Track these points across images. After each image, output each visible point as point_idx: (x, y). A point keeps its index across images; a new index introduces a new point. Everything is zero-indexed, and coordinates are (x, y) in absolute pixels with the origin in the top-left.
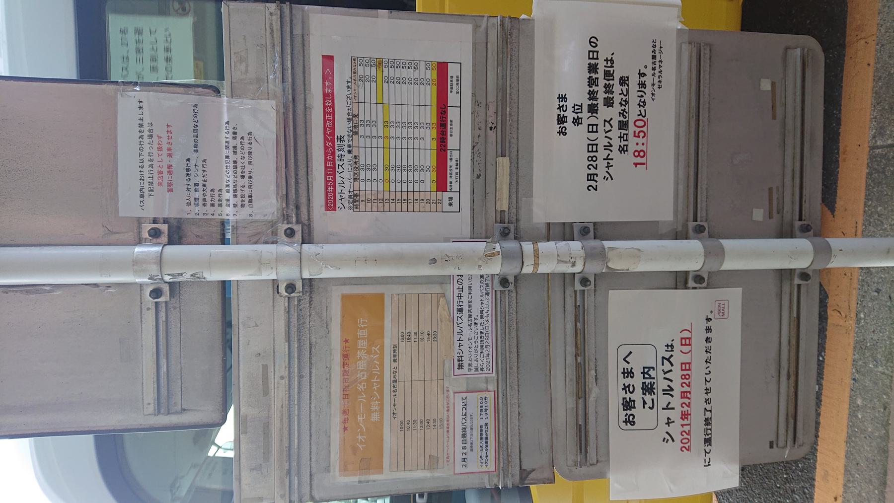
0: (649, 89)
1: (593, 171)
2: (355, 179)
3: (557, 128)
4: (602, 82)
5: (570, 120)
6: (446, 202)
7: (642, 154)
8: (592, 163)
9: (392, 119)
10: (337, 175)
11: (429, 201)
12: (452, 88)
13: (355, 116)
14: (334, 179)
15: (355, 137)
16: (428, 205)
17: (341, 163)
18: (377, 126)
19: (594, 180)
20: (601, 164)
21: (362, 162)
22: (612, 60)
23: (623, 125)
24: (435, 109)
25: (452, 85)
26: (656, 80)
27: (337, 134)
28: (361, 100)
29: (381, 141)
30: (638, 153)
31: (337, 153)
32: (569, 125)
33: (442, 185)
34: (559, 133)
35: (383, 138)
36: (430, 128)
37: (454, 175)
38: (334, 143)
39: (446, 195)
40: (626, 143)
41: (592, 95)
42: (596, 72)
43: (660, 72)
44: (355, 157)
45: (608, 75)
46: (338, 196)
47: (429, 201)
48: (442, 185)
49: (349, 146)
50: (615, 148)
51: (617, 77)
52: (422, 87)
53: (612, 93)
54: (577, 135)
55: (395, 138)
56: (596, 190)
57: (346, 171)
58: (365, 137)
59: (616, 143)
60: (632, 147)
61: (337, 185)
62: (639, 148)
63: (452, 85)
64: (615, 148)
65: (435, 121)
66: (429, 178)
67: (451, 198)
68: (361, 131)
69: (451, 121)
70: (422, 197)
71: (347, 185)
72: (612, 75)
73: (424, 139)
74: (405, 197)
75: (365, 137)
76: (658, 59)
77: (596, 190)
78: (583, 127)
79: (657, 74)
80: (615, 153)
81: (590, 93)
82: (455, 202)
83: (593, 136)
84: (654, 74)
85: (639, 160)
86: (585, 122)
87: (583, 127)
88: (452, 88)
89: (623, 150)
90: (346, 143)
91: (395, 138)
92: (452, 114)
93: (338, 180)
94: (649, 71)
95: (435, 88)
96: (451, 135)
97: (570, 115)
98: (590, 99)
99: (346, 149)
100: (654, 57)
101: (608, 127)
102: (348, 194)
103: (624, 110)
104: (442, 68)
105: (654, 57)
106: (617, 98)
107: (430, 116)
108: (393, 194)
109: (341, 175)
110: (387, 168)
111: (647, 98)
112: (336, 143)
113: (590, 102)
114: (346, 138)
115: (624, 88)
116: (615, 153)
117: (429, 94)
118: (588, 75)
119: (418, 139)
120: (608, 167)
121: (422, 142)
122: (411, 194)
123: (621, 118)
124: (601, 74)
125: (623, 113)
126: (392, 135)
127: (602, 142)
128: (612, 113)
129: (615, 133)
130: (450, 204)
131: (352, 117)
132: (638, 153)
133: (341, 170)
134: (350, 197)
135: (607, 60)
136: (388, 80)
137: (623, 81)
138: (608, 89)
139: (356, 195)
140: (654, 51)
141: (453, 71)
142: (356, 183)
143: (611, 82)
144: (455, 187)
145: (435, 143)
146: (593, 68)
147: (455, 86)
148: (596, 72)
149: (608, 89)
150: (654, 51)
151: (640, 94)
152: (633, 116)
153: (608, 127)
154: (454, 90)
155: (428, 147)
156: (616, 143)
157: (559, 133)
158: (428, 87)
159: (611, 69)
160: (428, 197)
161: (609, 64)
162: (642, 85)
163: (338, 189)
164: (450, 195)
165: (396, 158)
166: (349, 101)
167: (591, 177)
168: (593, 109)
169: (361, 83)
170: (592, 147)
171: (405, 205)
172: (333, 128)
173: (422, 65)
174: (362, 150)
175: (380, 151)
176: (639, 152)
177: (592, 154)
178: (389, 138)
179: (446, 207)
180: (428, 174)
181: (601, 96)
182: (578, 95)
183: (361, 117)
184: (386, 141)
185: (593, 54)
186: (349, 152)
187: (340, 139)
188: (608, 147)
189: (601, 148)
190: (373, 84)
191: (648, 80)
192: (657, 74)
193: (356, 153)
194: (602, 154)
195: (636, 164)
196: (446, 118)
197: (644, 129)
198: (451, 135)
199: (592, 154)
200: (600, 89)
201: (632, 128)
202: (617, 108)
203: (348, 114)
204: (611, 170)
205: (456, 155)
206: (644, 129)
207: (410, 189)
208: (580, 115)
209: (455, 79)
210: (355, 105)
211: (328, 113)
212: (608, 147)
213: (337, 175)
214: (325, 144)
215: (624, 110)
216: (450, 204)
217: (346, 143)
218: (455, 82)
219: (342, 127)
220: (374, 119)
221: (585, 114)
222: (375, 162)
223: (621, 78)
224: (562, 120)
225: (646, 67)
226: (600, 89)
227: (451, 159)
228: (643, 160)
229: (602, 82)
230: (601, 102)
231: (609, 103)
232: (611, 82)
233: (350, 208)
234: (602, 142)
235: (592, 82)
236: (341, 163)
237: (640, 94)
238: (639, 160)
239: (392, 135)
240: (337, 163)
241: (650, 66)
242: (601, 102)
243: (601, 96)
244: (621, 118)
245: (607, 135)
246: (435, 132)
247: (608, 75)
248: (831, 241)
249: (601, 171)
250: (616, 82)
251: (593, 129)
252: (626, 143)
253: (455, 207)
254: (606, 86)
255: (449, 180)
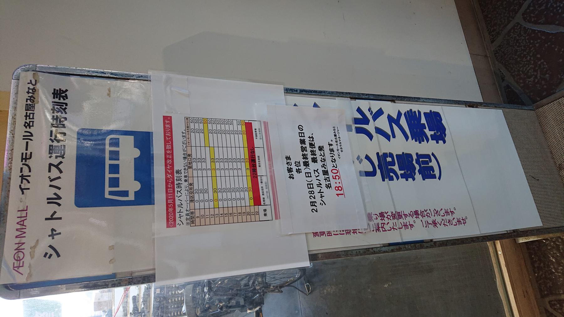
0: (336, 152)
1: (313, 200)
2: (191, 201)
3: (288, 175)
4: (309, 149)
5: (294, 170)
6: (262, 213)
7: (340, 188)
8: (311, 195)
9: (217, 157)
10: (177, 198)
11: (249, 214)
12: (256, 136)
13: (189, 155)
14: (174, 201)
15: (190, 170)
16: (249, 217)
17: (179, 190)
18: (206, 162)
19: (314, 205)
20: (318, 196)
21: (196, 187)
22: (312, 137)
23: (325, 173)
24: (246, 150)
25: (256, 134)
26: (339, 147)
27: (176, 168)
28: (193, 144)
29: (209, 172)
30: (338, 188)
31: (176, 182)
32: (294, 172)
33: (257, 201)
34: (290, 177)
35: (211, 169)
36: (245, 162)
37: (265, 193)
38: (173, 175)
39: (261, 208)
40: (329, 182)
41: (305, 156)
42: (305, 144)
43: (340, 143)
44: (191, 184)
45: (312, 145)
46: (177, 215)
47: (249, 214)
48: (257, 201)
49: (185, 176)
50: (323, 186)
51: (317, 146)
52: (236, 135)
53: (315, 155)
54: (301, 178)
55: (220, 169)
56: (317, 211)
57: (183, 195)
58: (197, 170)
59: (324, 183)
60: (333, 185)
61: (177, 206)
62: (338, 185)
63: (256, 134)
64: (323, 186)
65: (247, 157)
66: (248, 195)
67: (265, 210)
68: (194, 165)
69: (259, 157)
70: (244, 211)
71: (184, 206)
72: (314, 145)
73: (241, 169)
74: (230, 212)
75: (197, 170)
76: (338, 136)
77: (317, 211)
78: (303, 174)
79: (339, 145)
80: (324, 189)
81: (303, 155)
82: (268, 212)
83: (309, 179)
84: (337, 145)
85: (339, 192)
86: (304, 171)
87: (303, 174)
88: (256, 136)
89: (328, 186)
90: (183, 175)
91: (220, 169)
92: (258, 152)
93: (177, 203)
94: (334, 143)
95: (245, 136)
96: (260, 166)
97: (294, 168)
98: (303, 158)
99: (183, 179)
100: (335, 135)
101: (317, 174)
102: (185, 212)
103: (324, 164)
104: (249, 126)
105: (335, 135)
106: (319, 158)
107: (244, 153)
108: (221, 210)
109: (180, 198)
110: (215, 191)
111: (336, 157)
112: (175, 175)
113: (304, 160)
114: (183, 171)
115: (322, 152)
116: (324, 189)
117: (242, 140)
118: (301, 145)
119: (237, 169)
120: (321, 197)
121: (240, 171)
122: (235, 209)
123: (323, 169)
124: (307, 145)
125: (323, 166)
126: (217, 167)
127: (315, 183)
128: (318, 166)
129: (322, 177)
130: (265, 215)
131: (187, 156)
132: (338, 188)
133: (179, 194)
134: (187, 215)
135: (309, 137)
136: (211, 132)
137: (321, 148)
138: (313, 153)
139: (192, 213)
140: (335, 132)
141: (255, 126)
142: (192, 204)
143: (314, 149)
144: (267, 202)
145: (249, 172)
146: (303, 142)
147: (258, 135)
148: (305, 144)
149: (313, 153)
150: (335, 132)
151: (332, 155)
152: (329, 168)
153: (317, 174)
154: (258, 137)
155: (244, 174)
156: (324, 183)
157: (290, 177)
158: (240, 136)
159: (313, 142)
160: (248, 210)
161: (311, 140)
162: (332, 150)
163: (178, 209)
164: (265, 207)
165: (221, 184)
166: (184, 146)
167: (313, 204)
168: (306, 164)
169: (193, 134)
170: (310, 185)
171: (231, 218)
172: (172, 165)
173: (235, 122)
174: (195, 179)
175: (210, 179)
176: (338, 188)
177: (311, 190)
178: (215, 169)
179: (262, 217)
180: (246, 193)
181: (310, 157)
182: (297, 156)
183: (194, 156)
184: (213, 172)
185: (301, 134)
186: (186, 181)
187: (178, 172)
188: (319, 185)
189: (315, 186)
190: (202, 135)
191: (334, 147)
192: (339, 145)
193: (190, 181)
194: (316, 189)
195: (338, 195)
196: (255, 155)
197: (338, 174)
198: (260, 166)
199: (311, 190)
200: (309, 153)
201: (331, 174)
202: (320, 164)
203: (184, 154)
204: (323, 199)
205: (264, 179)
206: (338, 174)
207: (234, 205)
208: (300, 168)
209: (257, 130)
210: (189, 148)
211: (169, 154)
212: (319, 185)
213: (176, 198)
214: (166, 176)
215: (324, 164)
216: (265, 215)
217: (183, 175)
218: (258, 132)
219: (179, 164)
220: (203, 157)
221: (302, 167)
222: (205, 187)
223: (319, 147)
224: (290, 170)
225: (332, 141)
226: (309, 153)
227: (262, 182)
228: (341, 192)
229: (309, 149)
230: (310, 160)
231: (314, 160)
232: (314, 149)
233: (188, 224)
234: (315, 183)
235: (303, 149)
236: (179, 190)
237: (332, 155)
238: (339, 192)
239: (217, 167)
240: (176, 189)
241: (334, 140)
242: (310, 160)
243: (310, 157)
244: (323, 169)
245: (317, 178)
246: (248, 164)
247: (312, 145)
248: (307, 264)
249: (318, 200)
250: (317, 149)
251: (308, 175)
252: (329, 182)
253: (269, 217)
254: (311, 151)
255: (262, 197)
